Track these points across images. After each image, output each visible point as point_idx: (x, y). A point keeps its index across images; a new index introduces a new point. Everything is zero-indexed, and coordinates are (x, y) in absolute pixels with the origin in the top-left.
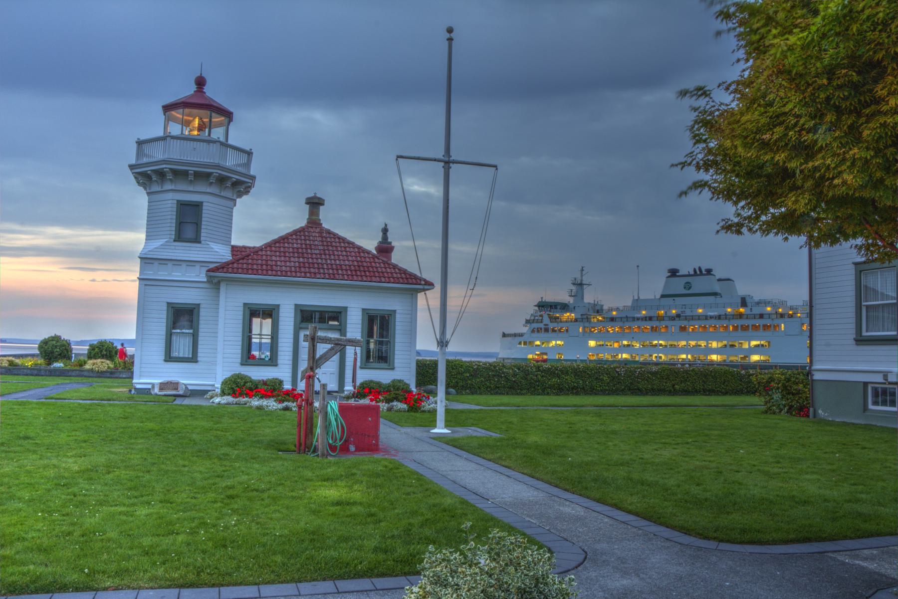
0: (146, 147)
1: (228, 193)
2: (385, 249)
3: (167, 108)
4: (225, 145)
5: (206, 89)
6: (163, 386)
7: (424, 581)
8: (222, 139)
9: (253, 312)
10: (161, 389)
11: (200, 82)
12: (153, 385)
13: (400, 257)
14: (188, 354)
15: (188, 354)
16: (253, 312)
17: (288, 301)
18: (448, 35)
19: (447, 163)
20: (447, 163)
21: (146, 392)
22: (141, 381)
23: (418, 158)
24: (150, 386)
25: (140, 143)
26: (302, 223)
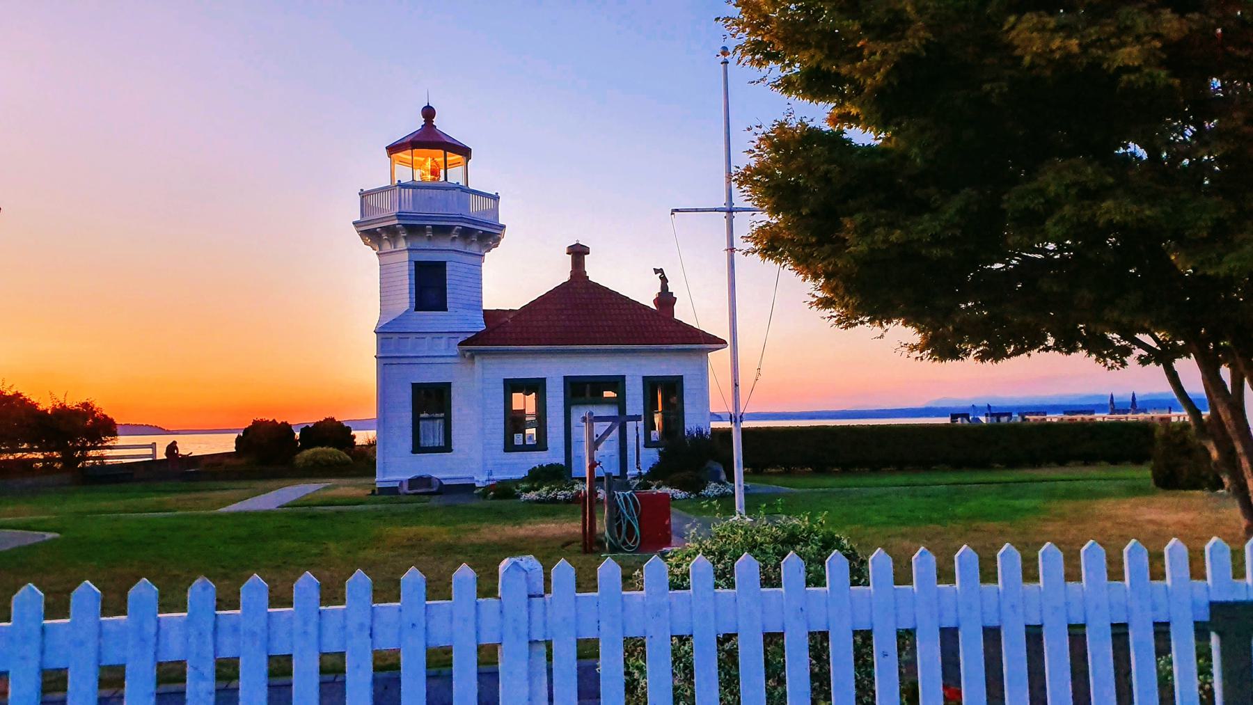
0: (371, 200)
1: (474, 248)
2: (666, 299)
3: (393, 149)
4: (465, 190)
5: (436, 121)
6: (413, 483)
7: (1240, 123)
8: (462, 183)
9: (512, 386)
10: (410, 488)
11: (429, 113)
12: (401, 482)
13: (682, 313)
14: (439, 441)
15: (439, 441)
16: (512, 386)
17: (554, 369)
18: (722, 58)
19: (730, 211)
20: (730, 211)
21: (393, 491)
22: (383, 478)
23: (697, 210)
24: (397, 485)
25: (364, 195)
26: (566, 277)
